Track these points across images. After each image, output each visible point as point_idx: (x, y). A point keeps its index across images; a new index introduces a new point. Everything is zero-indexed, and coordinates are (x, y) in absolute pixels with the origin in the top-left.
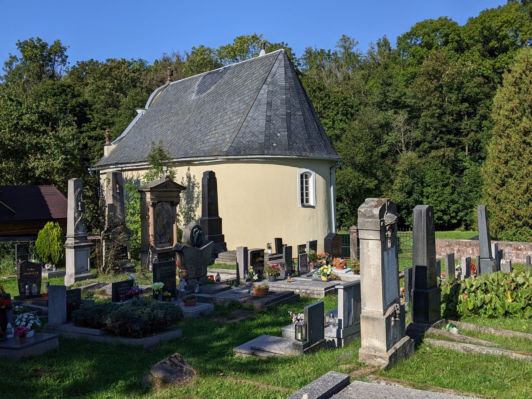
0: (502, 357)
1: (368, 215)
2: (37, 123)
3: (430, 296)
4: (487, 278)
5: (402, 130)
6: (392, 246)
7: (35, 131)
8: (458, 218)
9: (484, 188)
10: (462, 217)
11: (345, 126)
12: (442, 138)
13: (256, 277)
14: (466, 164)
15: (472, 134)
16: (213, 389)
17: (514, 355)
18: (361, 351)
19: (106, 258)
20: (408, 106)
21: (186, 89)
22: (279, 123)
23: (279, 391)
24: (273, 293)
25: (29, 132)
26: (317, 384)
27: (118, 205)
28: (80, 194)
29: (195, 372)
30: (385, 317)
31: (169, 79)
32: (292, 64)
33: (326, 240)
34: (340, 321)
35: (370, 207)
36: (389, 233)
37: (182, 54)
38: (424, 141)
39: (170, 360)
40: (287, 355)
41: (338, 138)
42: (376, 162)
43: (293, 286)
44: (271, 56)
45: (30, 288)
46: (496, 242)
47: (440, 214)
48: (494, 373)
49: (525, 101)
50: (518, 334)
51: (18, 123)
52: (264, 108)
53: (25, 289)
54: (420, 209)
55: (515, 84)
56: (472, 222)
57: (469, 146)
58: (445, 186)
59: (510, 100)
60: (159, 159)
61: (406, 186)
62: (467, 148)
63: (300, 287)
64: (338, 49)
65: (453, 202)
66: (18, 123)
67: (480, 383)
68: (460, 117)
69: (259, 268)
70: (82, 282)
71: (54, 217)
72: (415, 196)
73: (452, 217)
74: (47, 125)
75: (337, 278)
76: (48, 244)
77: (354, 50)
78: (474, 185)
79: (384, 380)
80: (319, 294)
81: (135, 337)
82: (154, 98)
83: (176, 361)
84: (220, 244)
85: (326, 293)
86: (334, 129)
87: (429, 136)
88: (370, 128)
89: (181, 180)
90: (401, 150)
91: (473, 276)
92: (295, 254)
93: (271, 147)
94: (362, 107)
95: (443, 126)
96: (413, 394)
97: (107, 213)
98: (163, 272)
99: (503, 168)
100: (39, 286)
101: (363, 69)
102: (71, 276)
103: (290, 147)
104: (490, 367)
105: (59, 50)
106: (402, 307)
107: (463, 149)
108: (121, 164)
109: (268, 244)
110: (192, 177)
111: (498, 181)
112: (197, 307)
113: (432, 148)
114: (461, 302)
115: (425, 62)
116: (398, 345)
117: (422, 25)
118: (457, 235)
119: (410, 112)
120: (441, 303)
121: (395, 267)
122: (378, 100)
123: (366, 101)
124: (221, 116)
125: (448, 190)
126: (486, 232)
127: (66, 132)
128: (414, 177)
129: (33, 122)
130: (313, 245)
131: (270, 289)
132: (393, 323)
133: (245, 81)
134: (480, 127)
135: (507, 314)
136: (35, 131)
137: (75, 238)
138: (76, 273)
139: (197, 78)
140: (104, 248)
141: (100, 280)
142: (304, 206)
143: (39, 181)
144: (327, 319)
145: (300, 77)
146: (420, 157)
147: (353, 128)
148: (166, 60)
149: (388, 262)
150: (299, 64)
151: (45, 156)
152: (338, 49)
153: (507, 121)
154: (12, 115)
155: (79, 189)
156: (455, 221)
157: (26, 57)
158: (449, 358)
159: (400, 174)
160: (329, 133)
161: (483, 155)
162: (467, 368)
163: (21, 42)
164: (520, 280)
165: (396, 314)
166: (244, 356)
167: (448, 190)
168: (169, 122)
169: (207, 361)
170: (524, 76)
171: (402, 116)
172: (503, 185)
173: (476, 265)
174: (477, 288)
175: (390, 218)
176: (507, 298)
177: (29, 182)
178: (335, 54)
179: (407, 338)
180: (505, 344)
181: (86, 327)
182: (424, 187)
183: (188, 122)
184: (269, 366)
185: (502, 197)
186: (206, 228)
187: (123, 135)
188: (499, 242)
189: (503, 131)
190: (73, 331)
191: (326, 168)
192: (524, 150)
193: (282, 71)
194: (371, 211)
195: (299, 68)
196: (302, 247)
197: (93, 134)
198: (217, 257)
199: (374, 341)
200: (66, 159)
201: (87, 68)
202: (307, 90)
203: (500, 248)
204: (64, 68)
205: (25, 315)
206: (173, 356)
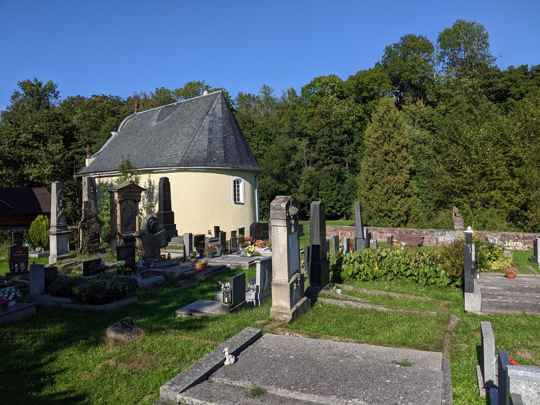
0: (372, 310)
1: (277, 208)
2: (32, 140)
3: (322, 266)
4: (361, 253)
5: (305, 151)
6: (295, 231)
7: (30, 147)
8: (342, 211)
9: (358, 191)
10: (344, 211)
11: (265, 148)
12: (331, 158)
13: (198, 255)
14: (346, 175)
15: (351, 155)
16: (155, 345)
17: (381, 309)
18: (272, 309)
19: (82, 242)
20: (309, 136)
21: (149, 117)
22: (217, 144)
23: (208, 344)
24: (210, 267)
25: (25, 147)
26: (237, 338)
27: (92, 202)
28: (61, 193)
29: (142, 332)
30: (290, 283)
31: (136, 110)
32: (228, 104)
33: (251, 227)
34: (258, 286)
35: (279, 203)
36: (293, 221)
37: (148, 93)
38: (319, 159)
39: (121, 323)
40: (217, 314)
41: (261, 156)
42: (287, 173)
43: (226, 262)
44: (212, 95)
45: (19, 266)
46: (366, 228)
47: (329, 209)
48: (366, 322)
49: (386, 132)
50: (383, 292)
51: (16, 140)
52: (206, 133)
53: (15, 267)
54: (315, 204)
55: (380, 121)
56: (351, 214)
57: (349, 163)
58: (333, 190)
59: (376, 131)
60: (127, 168)
61: (307, 190)
62: (347, 164)
63: (231, 262)
64: (261, 94)
65: (338, 201)
66: (16, 140)
67: (357, 330)
68: (342, 144)
69: (202, 249)
70: (62, 261)
71: (44, 212)
72: (313, 197)
73: (337, 211)
74: (39, 142)
75: (258, 254)
76: (39, 231)
77: (272, 95)
78: (352, 189)
79: (288, 331)
80: (245, 267)
81: (99, 304)
83: (126, 323)
84: (172, 230)
85: (249, 265)
86: (259, 150)
87: (322, 157)
88: (283, 150)
89: (144, 184)
90: (304, 166)
91: (351, 251)
92: (228, 238)
93: (212, 161)
94: (278, 135)
95: (332, 150)
96: (308, 342)
97: (83, 208)
98: (126, 251)
99: (371, 178)
100: (26, 264)
101: (278, 109)
102: (54, 256)
103: (226, 161)
104: (364, 318)
105: (51, 88)
106: (302, 276)
107: (345, 165)
108: (99, 172)
109: (209, 231)
110: (152, 181)
111: (368, 186)
112: (151, 279)
113: (325, 164)
114: (343, 270)
115: (319, 106)
116: (299, 304)
117: (319, 80)
118: (341, 223)
119: (310, 140)
120: (330, 271)
121: (297, 246)
122: (288, 130)
123: (280, 131)
124: (174, 138)
125: (335, 193)
126: (360, 220)
127: (54, 148)
128: (312, 184)
129: (28, 139)
130: (242, 231)
131: (209, 264)
132: (295, 288)
133: (193, 113)
134: (356, 150)
135: (375, 278)
136: (30, 147)
137: (57, 227)
138: (58, 254)
139: (157, 110)
140: (81, 235)
141: (77, 259)
142: (236, 203)
143: (33, 184)
144: (249, 285)
145: (234, 113)
146: (316, 170)
147: (271, 150)
148: (136, 97)
149: (292, 242)
150: (234, 104)
151: (37, 165)
152: (261, 94)
153: (374, 145)
154: (11, 134)
155: (60, 190)
156: (340, 214)
157: (26, 93)
158: (335, 312)
159: (303, 181)
160: (255, 153)
161: (358, 169)
162: (348, 319)
164: (384, 254)
165: (297, 281)
166: (184, 316)
167: (335, 193)
168: (135, 142)
169: (155, 321)
170: (385, 116)
171: (305, 142)
172: (371, 189)
173: (354, 243)
174: (355, 260)
175: (293, 210)
176: (375, 267)
177: (25, 185)
178: (258, 97)
179: (305, 298)
180: (374, 300)
181: (59, 297)
182: (319, 190)
183: (149, 142)
184: (202, 323)
185: (371, 197)
186: (162, 220)
187: (101, 150)
188: (369, 227)
189: (371, 153)
190: (50, 300)
191: (252, 176)
192: (385, 165)
193: (220, 106)
194: (280, 205)
195: (234, 106)
196: (234, 233)
197: (79, 150)
198: (170, 240)
199: (281, 302)
200: (54, 168)
201: (75, 101)
202: (240, 122)
203: (370, 231)
204: (57, 101)
205: (8, 289)
206: (124, 319)
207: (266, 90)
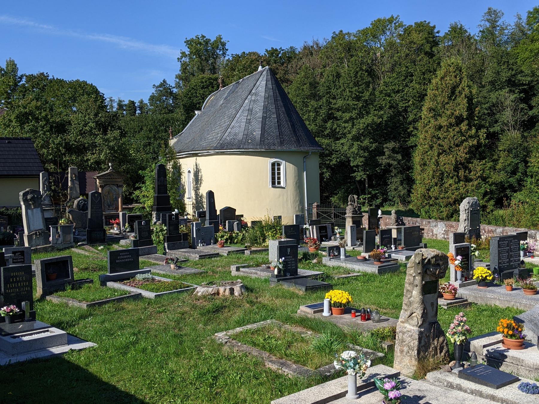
2: (95, 129)
82: (207, 102)
105: (220, 44)
142: (273, 187)
163: (188, 39)
207: (493, 16)
